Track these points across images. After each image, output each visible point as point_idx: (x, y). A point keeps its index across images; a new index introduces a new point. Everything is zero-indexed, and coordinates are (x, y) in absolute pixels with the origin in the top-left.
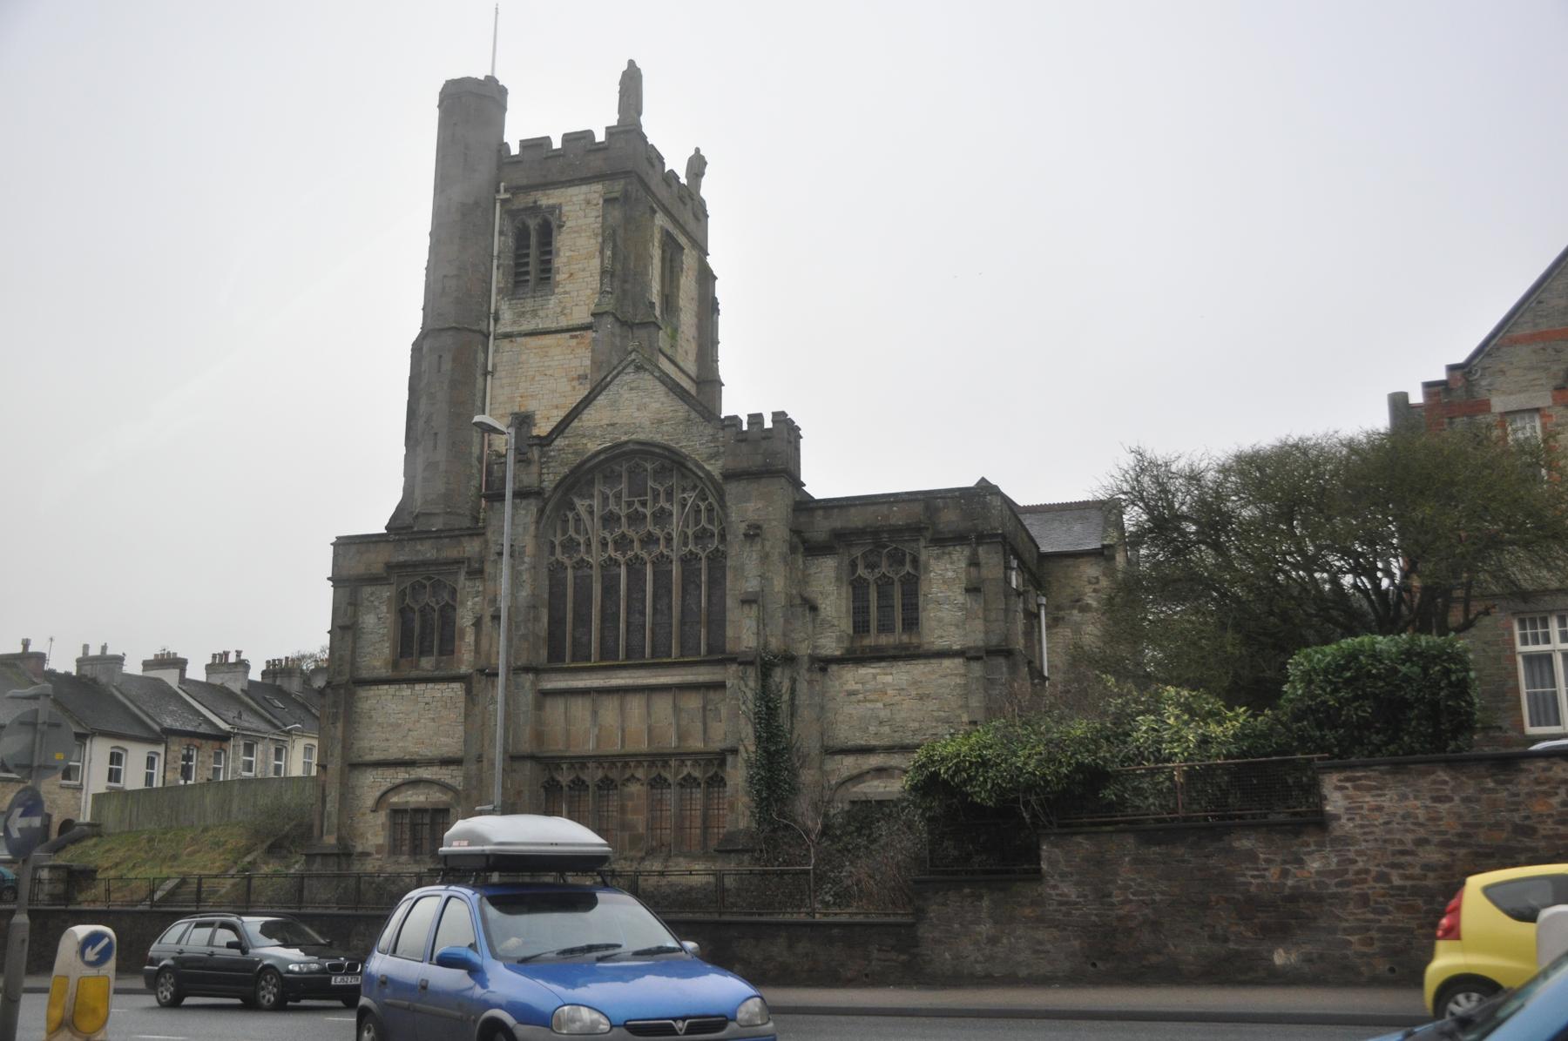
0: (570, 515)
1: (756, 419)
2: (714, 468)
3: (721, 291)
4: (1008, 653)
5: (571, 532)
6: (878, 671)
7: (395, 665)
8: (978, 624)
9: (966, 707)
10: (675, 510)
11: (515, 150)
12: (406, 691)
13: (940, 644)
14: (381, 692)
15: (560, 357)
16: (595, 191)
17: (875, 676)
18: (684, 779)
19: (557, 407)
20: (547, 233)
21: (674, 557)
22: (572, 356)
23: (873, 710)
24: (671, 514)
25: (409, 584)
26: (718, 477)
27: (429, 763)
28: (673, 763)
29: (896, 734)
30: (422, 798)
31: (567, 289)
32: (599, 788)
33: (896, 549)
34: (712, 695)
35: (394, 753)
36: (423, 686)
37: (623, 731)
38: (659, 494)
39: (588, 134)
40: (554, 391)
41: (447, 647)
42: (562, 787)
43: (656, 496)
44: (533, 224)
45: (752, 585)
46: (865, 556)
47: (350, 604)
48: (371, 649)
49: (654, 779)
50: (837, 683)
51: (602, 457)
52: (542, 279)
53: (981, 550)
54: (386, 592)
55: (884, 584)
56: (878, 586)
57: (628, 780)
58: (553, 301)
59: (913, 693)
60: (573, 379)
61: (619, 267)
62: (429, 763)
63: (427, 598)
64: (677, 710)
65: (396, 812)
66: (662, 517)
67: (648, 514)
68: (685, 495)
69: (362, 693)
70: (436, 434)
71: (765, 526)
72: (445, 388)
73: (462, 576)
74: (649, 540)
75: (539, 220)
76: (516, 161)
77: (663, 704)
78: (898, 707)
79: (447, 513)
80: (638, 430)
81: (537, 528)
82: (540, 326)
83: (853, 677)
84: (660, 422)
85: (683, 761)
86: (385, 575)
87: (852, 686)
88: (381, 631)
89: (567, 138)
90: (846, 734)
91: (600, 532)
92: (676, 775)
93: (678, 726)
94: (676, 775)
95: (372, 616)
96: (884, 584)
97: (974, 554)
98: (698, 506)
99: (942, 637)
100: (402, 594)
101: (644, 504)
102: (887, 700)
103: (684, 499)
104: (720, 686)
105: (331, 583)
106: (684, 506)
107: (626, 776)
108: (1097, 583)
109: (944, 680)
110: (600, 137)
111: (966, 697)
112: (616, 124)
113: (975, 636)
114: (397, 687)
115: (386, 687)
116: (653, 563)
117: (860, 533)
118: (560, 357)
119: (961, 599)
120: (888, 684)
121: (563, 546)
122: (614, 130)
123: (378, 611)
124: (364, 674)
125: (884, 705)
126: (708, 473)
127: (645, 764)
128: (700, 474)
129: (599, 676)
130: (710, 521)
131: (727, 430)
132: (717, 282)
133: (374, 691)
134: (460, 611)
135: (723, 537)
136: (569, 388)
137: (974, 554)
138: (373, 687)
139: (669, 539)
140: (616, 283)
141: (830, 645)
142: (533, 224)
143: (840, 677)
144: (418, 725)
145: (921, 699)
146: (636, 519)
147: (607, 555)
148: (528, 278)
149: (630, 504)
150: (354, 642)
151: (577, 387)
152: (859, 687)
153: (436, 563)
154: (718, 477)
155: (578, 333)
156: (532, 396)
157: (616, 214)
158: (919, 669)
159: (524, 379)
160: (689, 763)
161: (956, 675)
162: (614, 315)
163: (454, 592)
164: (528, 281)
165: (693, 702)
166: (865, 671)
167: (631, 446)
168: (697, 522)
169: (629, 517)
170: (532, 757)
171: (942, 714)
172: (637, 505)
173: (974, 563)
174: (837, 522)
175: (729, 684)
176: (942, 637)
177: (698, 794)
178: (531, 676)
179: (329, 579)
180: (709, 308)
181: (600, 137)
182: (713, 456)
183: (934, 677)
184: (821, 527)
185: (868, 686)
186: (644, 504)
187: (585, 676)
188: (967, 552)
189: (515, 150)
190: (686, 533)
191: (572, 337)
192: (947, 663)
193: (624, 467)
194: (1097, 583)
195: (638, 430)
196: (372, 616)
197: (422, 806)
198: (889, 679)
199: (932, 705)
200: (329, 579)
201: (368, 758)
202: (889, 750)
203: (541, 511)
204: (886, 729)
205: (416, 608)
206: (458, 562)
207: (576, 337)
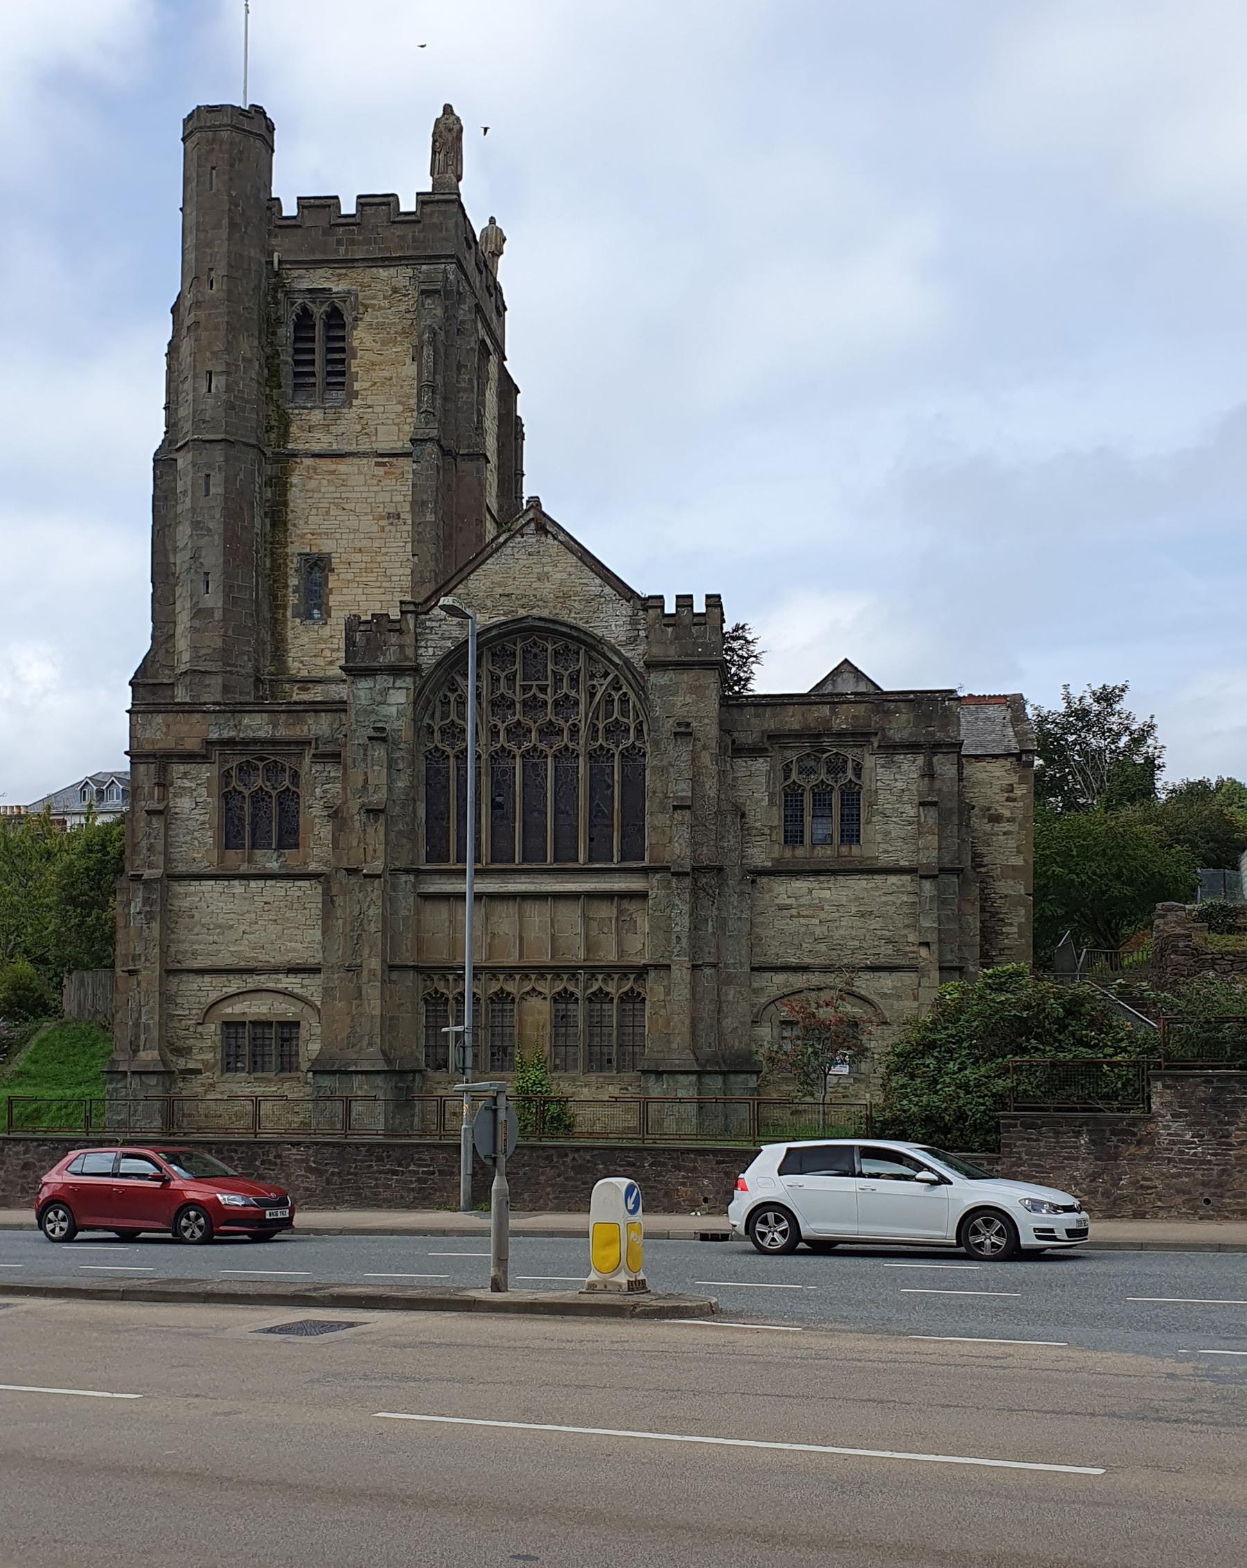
0: (452, 697)
1: (685, 601)
2: (636, 655)
3: (524, 407)
4: (959, 872)
5: (453, 716)
6: (815, 885)
7: (221, 860)
8: (933, 840)
9: (914, 926)
10: (583, 698)
11: (290, 209)
12: (238, 887)
13: (885, 860)
14: (203, 888)
15: (362, 489)
16: (399, 276)
17: (810, 891)
18: (594, 994)
19: (360, 551)
20: (335, 319)
21: (581, 749)
22: (379, 488)
23: (807, 925)
24: (577, 703)
25: (235, 764)
26: (639, 665)
27: (275, 971)
28: (582, 977)
29: (834, 952)
30: (264, 1010)
31: (370, 403)
32: (493, 1001)
33: (837, 754)
34: (632, 906)
35: (225, 959)
36: (261, 883)
37: (521, 939)
38: (561, 680)
39: (390, 200)
40: (356, 531)
41: (289, 837)
42: (447, 999)
43: (558, 680)
44: (319, 311)
45: (683, 789)
46: (800, 760)
47: (157, 784)
48: (188, 838)
49: (559, 993)
50: (767, 896)
51: (494, 632)
52: (329, 384)
53: (935, 759)
54: (206, 772)
55: (533, 758)
56: (814, 794)
57: (528, 993)
58: (350, 414)
59: (854, 910)
60: (382, 518)
61: (439, 380)
62: (275, 971)
63: (258, 781)
64: (587, 919)
65: (232, 1026)
66: (565, 704)
67: (550, 702)
68: (595, 683)
69: (179, 888)
70: (207, 574)
71: (694, 724)
72: (217, 516)
73: (307, 760)
74: (550, 731)
75: (325, 308)
76: (291, 225)
77: (570, 915)
78: (837, 924)
79: (226, 672)
80: (540, 603)
81: (415, 710)
82: (335, 447)
83: (785, 890)
84: (567, 596)
85: (593, 975)
86: (204, 752)
87: (783, 900)
88: (202, 818)
89: (364, 201)
90: (775, 952)
91: (490, 718)
92: (586, 988)
93: (587, 936)
94: (586, 988)
95: (187, 799)
96: (533, 758)
97: (930, 764)
98: (610, 695)
99: (888, 852)
100: (226, 776)
101: (543, 689)
102: (822, 915)
103: (594, 687)
104: (643, 896)
105: (129, 758)
106: (592, 695)
107: (526, 990)
108: (1012, 791)
109: (891, 898)
110: (408, 204)
111: (915, 917)
112: (430, 189)
113: (929, 857)
114: (226, 883)
115: (212, 882)
116: (555, 756)
117: (797, 735)
118: (362, 489)
119: (911, 811)
120: (826, 900)
121: (443, 731)
122: (426, 198)
123: (195, 794)
124: (182, 868)
125: (820, 921)
126: (627, 661)
127: (616, 977)
128: (617, 660)
129: (493, 880)
130: (625, 713)
131: (650, 611)
132: (519, 396)
133: (194, 887)
134: (305, 800)
135: (639, 731)
136: (375, 528)
137: (930, 764)
138: (193, 883)
139: (574, 731)
140: (439, 402)
141: (760, 856)
142: (319, 311)
143: (771, 891)
144: (256, 927)
145: (863, 916)
146: (533, 705)
147: (499, 745)
148: (312, 380)
149: (525, 689)
150: (167, 829)
151: (387, 529)
152: (792, 901)
153: (273, 742)
154: (639, 665)
155: (386, 460)
156: (326, 534)
157: (435, 308)
158: (859, 885)
159: (314, 512)
160: (600, 977)
161: (902, 893)
162: (438, 441)
163: (295, 776)
164: (314, 384)
165: (606, 911)
166: (800, 885)
167: (531, 623)
168: (609, 714)
169: (525, 703)
170: (416, 968)
171: (887, 933)
172: (534, 690)
173: (929, 774)
174: (770, 722)
175: (652, 894)
176: (888, 852)
177: (613, 1010)
178: (412, 878)
179: (126, 753)
180: (512, 431)
181: (408, 204)
182: (633, 641)
183: (877, 894)
184: (753, 727)
185: (802, 901)
186: (543, 689)
187: (524, 879)
188: (921, 760)
189: (290, 209)
190: (595, 725)
191: (378, 464)
192: (893, 879)
193: (519, 646)
194: (1012, 791)
195: (540, 603)
196: (187, 799)
197: (263, 1018)
198: (826, 894)
199: (875, 924)
200: (126, 753)
201: (188, 964)
202: (826, 969)
203: (419, 693)
204: (822, 947)
205: (247, 793)
206: (306, 743)
207: (384, 464)
